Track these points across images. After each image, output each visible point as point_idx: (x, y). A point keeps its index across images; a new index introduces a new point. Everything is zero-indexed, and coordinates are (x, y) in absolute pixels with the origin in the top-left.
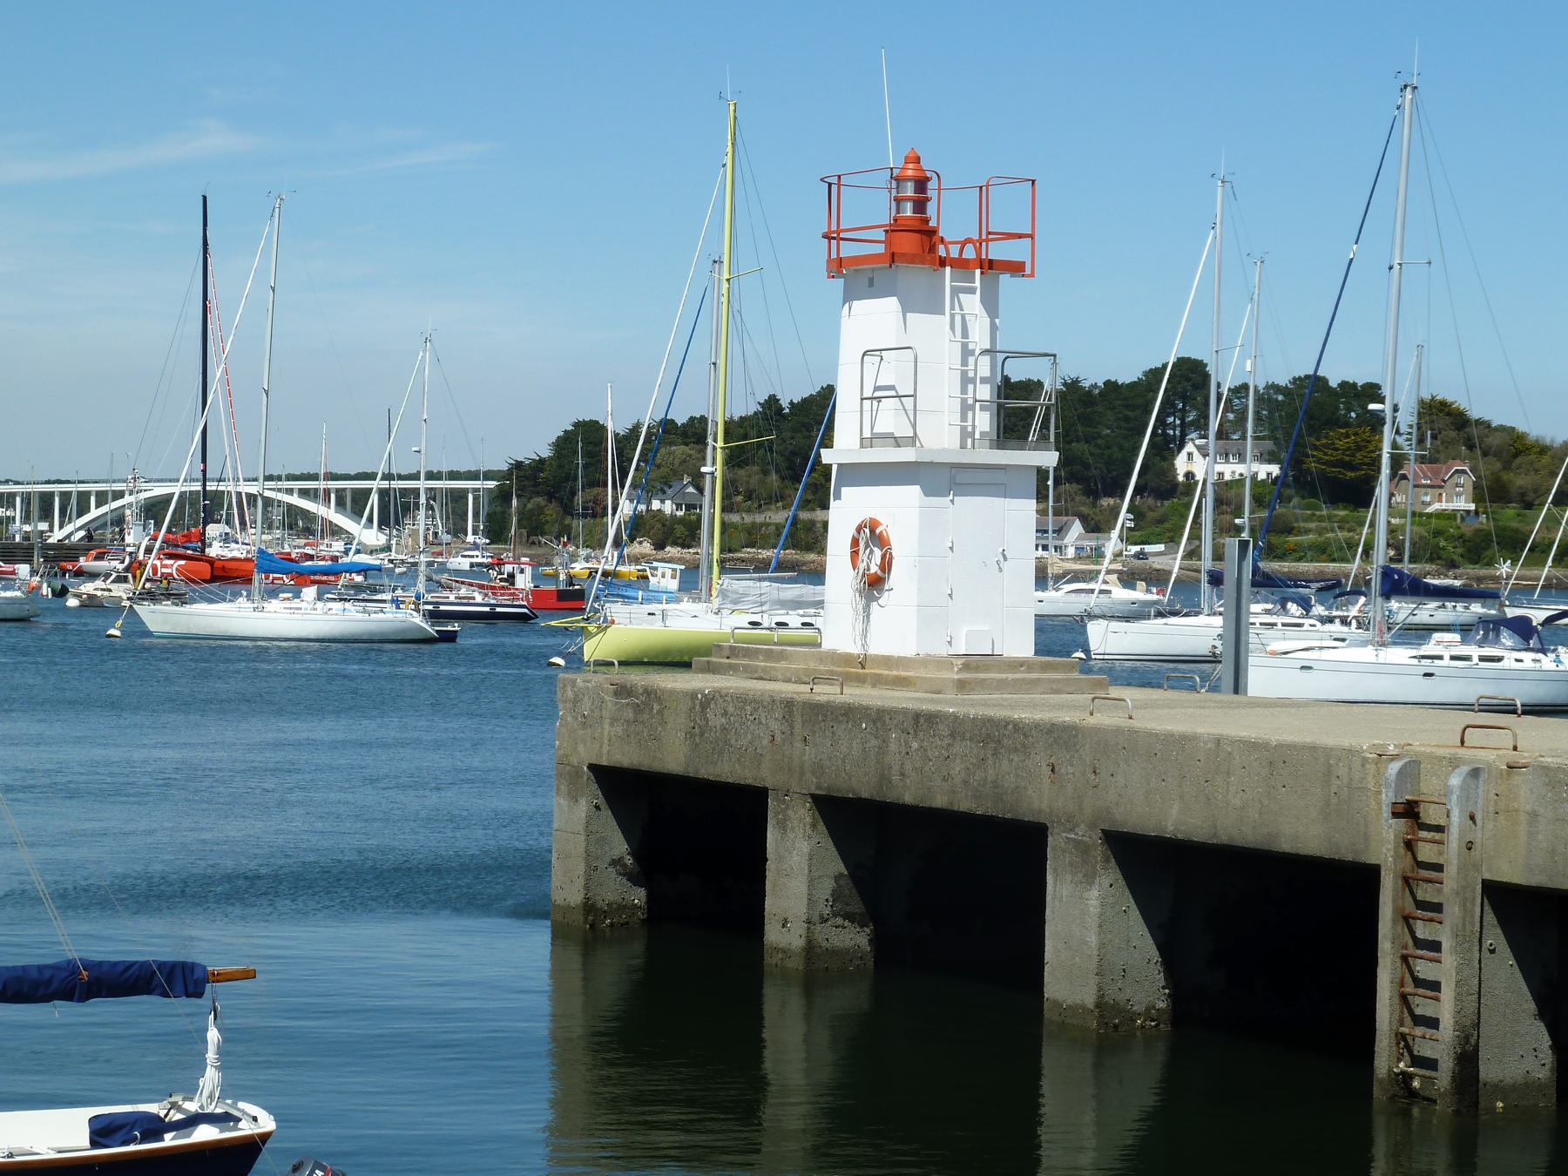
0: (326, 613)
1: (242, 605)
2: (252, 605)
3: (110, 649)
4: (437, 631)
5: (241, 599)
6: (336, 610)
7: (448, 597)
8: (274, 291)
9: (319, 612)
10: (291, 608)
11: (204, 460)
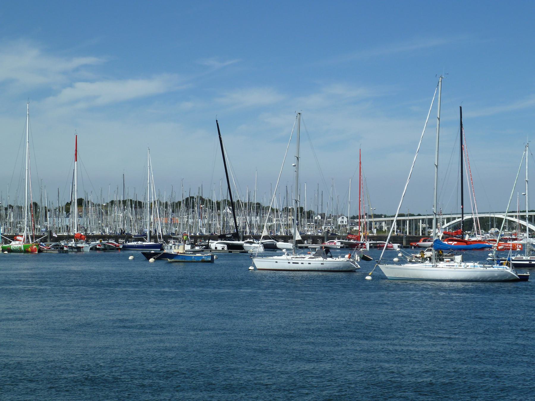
0: (466, 268)
1: (427, 265)
2: (431, 264)
3: (368, 287)
4: (519, 276)
5: (427, 262)
6: (471, 266)
7: (523, 258)
8: (439, 120)
9: (462, 267)
10: (449, 266)
11: (462, 204)
